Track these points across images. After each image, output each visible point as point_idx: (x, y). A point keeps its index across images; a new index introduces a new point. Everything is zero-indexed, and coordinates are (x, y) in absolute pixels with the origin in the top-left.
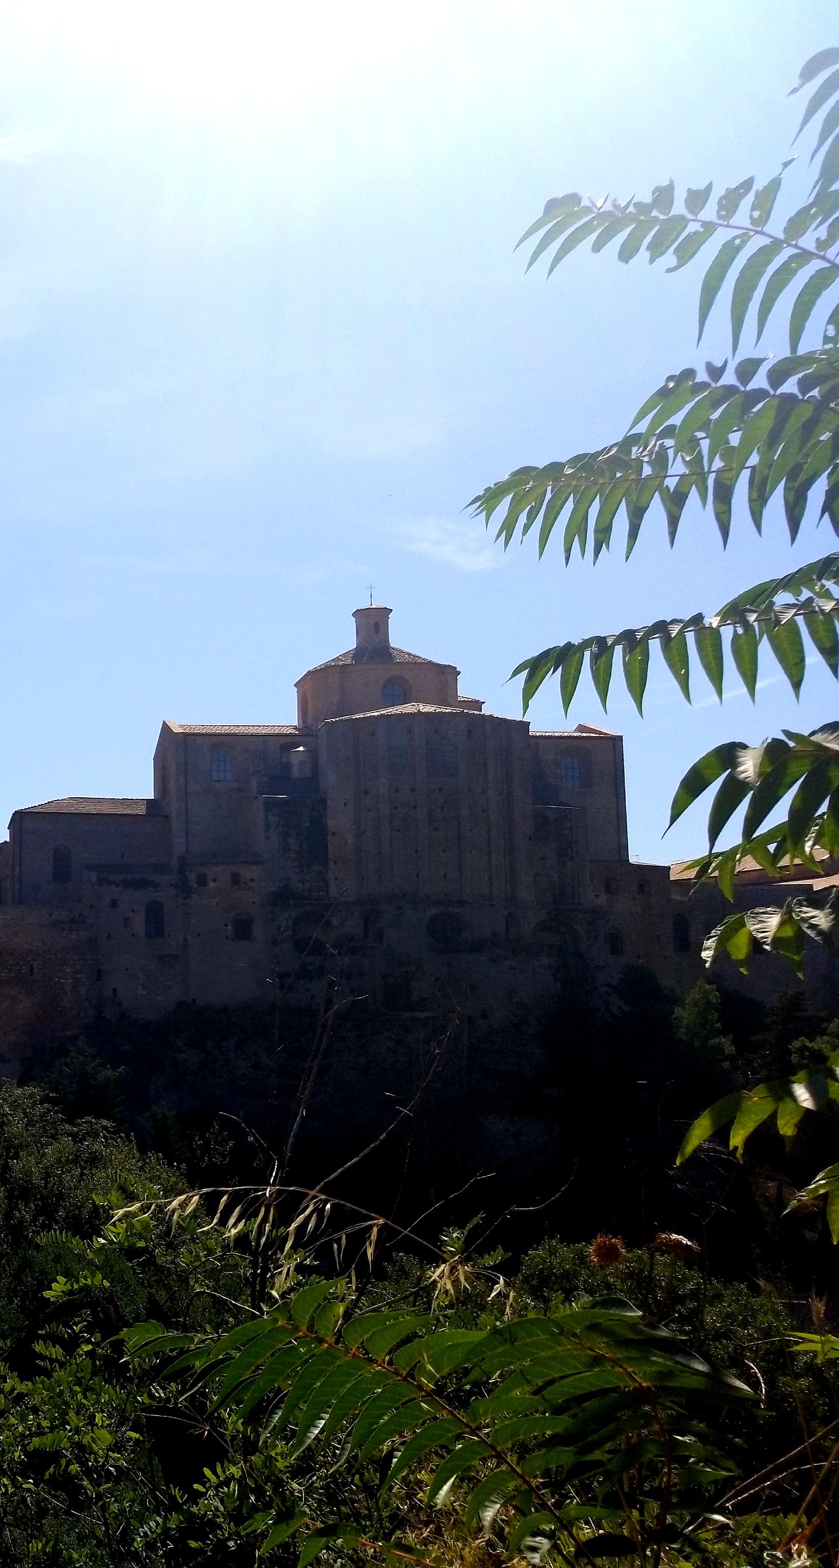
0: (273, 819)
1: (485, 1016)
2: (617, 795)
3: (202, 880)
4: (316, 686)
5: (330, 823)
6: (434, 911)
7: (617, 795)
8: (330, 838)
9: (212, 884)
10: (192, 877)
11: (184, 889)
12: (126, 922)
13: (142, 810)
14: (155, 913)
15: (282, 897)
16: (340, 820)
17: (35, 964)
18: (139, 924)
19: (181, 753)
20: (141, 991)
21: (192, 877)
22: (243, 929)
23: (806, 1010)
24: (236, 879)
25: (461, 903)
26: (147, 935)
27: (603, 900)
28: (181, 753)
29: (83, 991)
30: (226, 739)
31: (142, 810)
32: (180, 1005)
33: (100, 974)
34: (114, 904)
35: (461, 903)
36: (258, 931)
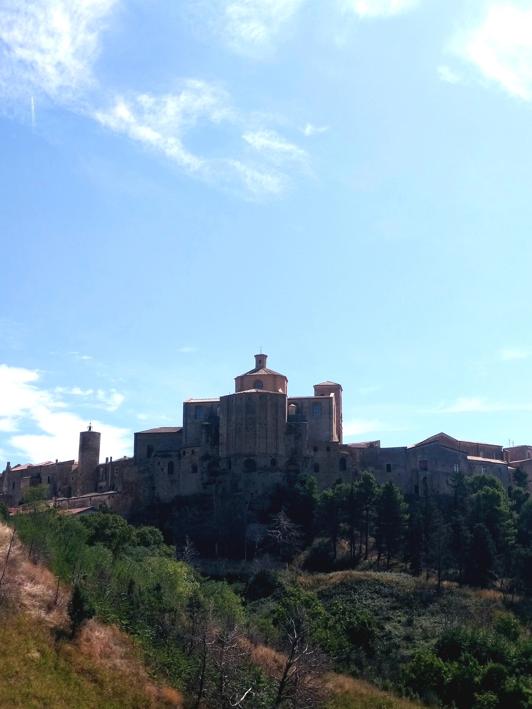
0: (204, 431)
1: (256, 493)
2: (330, 418)
3: (184, 454)
4: (241, 381)
5: (220, 431)
6: (245, 459)
7: (330, 418)
8: (220, 436)
9: (187, 454)
10: (182, 453)
11: (179, 457)
12: (162, 469)
13: (336, 439)
14: (171, 466)
15: (206, 457)
16: (223, 430)
17: (133, 486)
18: (166, 470)
19: (191, 410)
20: (166, 493)
21: (182, 453)
22: (195, 469)
23: (499, 506)
24: (193, 452)
25: (254, 456)
26: (168, 473)
27: (312, 453)
28: (191, 410)
29: (146, 494)
30: (200, 404)
31: (336, 439)
32: (177, 497)
33: (154, 488)
34: (159, 463)
35: (254, 456)
36: (157, 463)
